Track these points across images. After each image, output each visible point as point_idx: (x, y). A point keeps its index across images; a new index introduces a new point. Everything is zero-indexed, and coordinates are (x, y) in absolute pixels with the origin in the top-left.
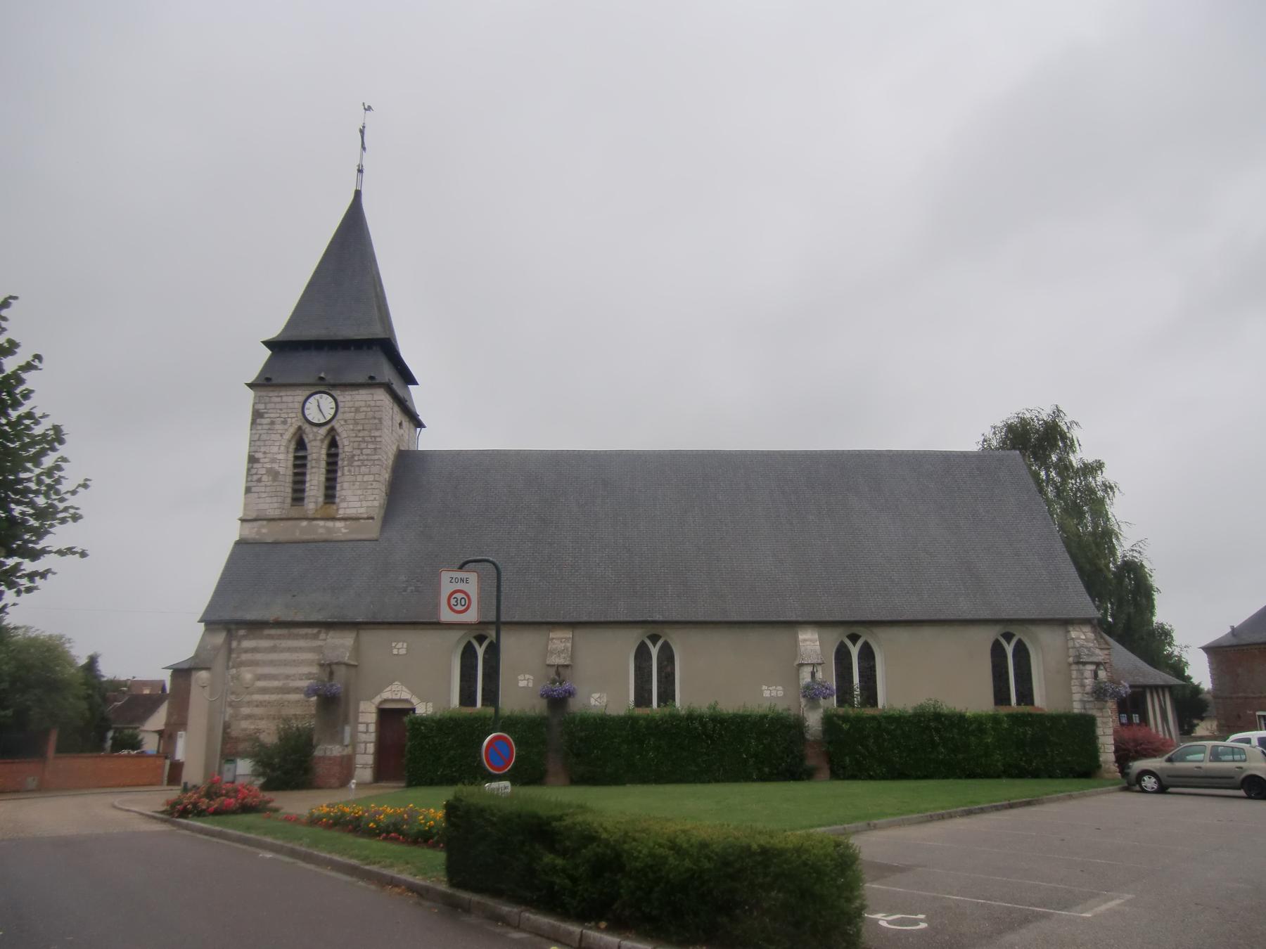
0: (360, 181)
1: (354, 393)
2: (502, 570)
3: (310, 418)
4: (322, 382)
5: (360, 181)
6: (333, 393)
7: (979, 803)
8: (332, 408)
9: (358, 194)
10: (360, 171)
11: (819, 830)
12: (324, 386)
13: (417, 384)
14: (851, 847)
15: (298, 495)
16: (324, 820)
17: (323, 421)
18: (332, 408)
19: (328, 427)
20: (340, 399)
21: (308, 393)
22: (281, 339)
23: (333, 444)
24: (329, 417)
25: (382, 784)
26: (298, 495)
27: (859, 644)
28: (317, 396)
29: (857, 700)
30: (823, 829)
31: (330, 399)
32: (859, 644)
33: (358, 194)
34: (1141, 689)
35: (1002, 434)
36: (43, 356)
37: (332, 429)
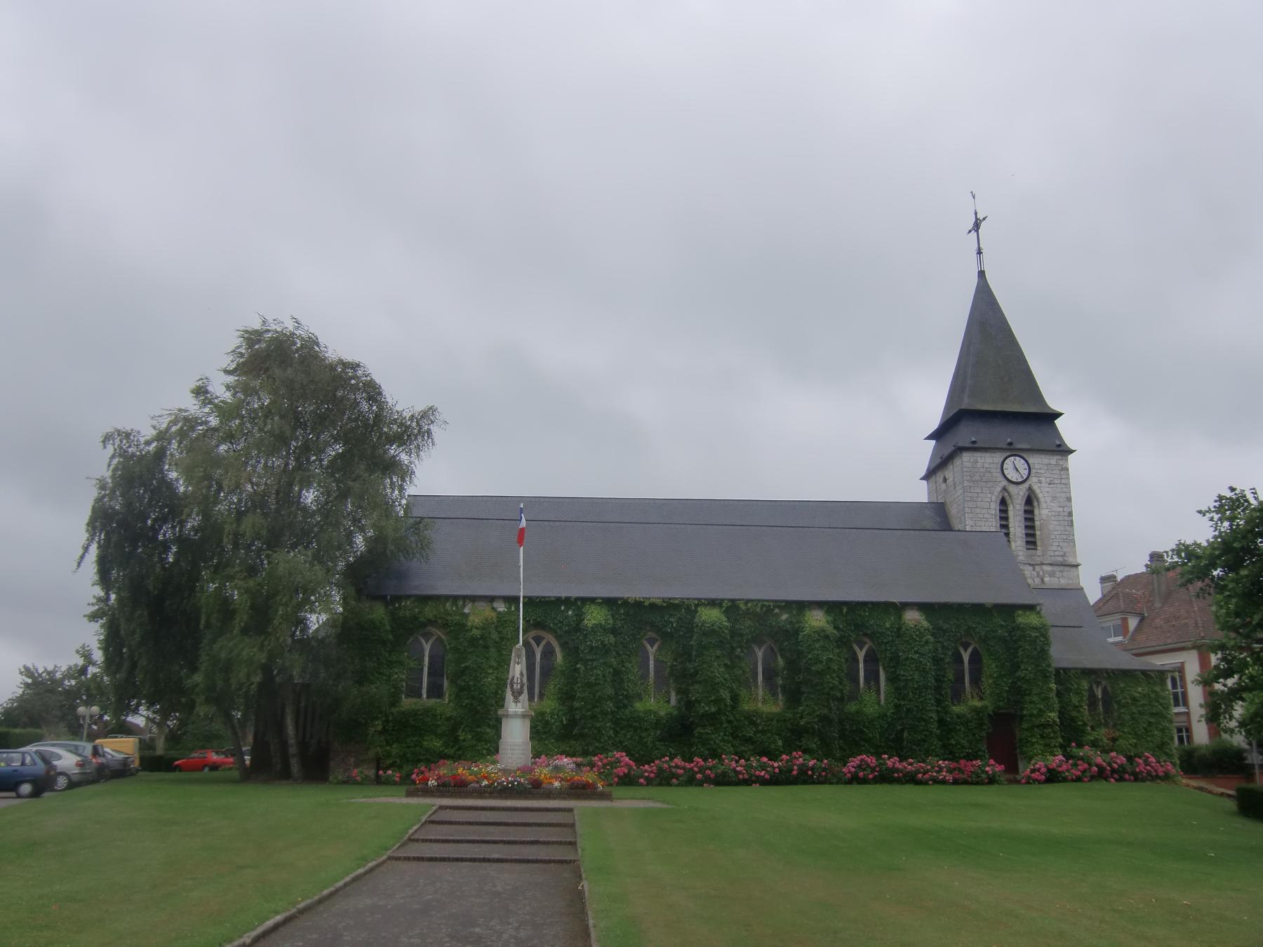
0: (980, 262)
1: (1051, 457)
5: (980, 262)
6: (1024, 456)
9: (982, 274)
10: (979, 252)
12: (1012, 450)
13: (1060, 414)
14: (559, 698)
17: (1020, 480)
18: (1026, 469)
19: (1026, 485)
20: (1031, 461)
21: (1008, 454)
22: (945, 420)
27: (970, 650)
28: (1012, 458)
29: (435, 638)
32: (970, 650)
33: (982, 274)
34: (1179, 665)
35: (839, 765)
36: (1149, 553)
37: (1030, 489)
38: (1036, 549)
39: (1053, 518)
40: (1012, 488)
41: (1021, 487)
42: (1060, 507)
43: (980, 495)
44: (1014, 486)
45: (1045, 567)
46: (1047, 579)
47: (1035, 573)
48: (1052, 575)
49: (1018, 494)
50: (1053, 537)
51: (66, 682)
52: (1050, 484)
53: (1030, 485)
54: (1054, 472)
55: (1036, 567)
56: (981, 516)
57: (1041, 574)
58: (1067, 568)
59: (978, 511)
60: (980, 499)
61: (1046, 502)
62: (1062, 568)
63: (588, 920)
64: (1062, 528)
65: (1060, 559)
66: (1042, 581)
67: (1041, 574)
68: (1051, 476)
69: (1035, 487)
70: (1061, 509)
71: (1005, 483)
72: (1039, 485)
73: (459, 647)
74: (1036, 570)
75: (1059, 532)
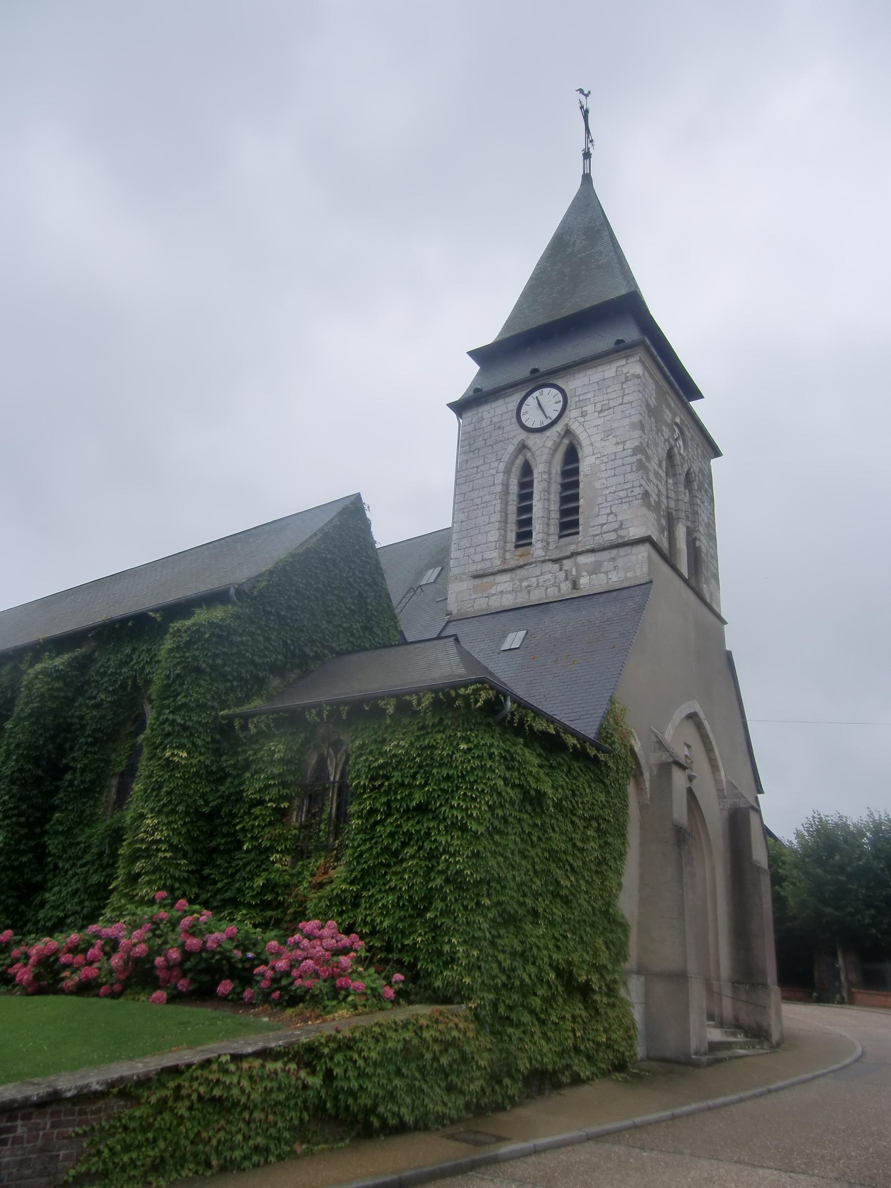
2: (514, 420)
3: (529, 424)
4: (537, 374)
6: (555, 382)
7: (52, 1152)
8: (559, 402)
9: (587, 179)
11: (694, 1106)
15: (524, 536)
16: (130, 624)
17: (547, 422)
19: (559, 428)
21: (524, 393)
23: (572, 456)
24: (554, 415)
25: (465, 1160)
26: (524, 536)
30: (686, 1108)
31: (554, 391)
33: (587, 179)
37: (568, 432)
38: (530, 544)
39: (603, 467)
40: (534, 441)
41: (548, 433)
42: (617, 444)
43: (483, 468)
44: (538, 435)
45: (582, 560)
46: (584, 581)
47: (561, 575)
48: (595, 570)
49: (543, 446)
50: (600, 500)
51: (96, 749)
52: (600, 412)
53: (567, 425)
54: (609, 390)
55: (565, 562)
56: (478, 501)
57: (574, 573)
58: (623, 551)
59: (475, 494)
60: (479, 475)
61: (592, 444)
62: (614, 552)
63: (170, 1051)
64: (621, 479)
65: (612, 536)
66: (575, 585)
67: (574, 573)
68: (606, 397)
69: (575, 427)
70: (621, 447)
71: (523, 435)
72: (582, 420)
73: (200, 719)
74: (565, 568)
75: (612, 489)
